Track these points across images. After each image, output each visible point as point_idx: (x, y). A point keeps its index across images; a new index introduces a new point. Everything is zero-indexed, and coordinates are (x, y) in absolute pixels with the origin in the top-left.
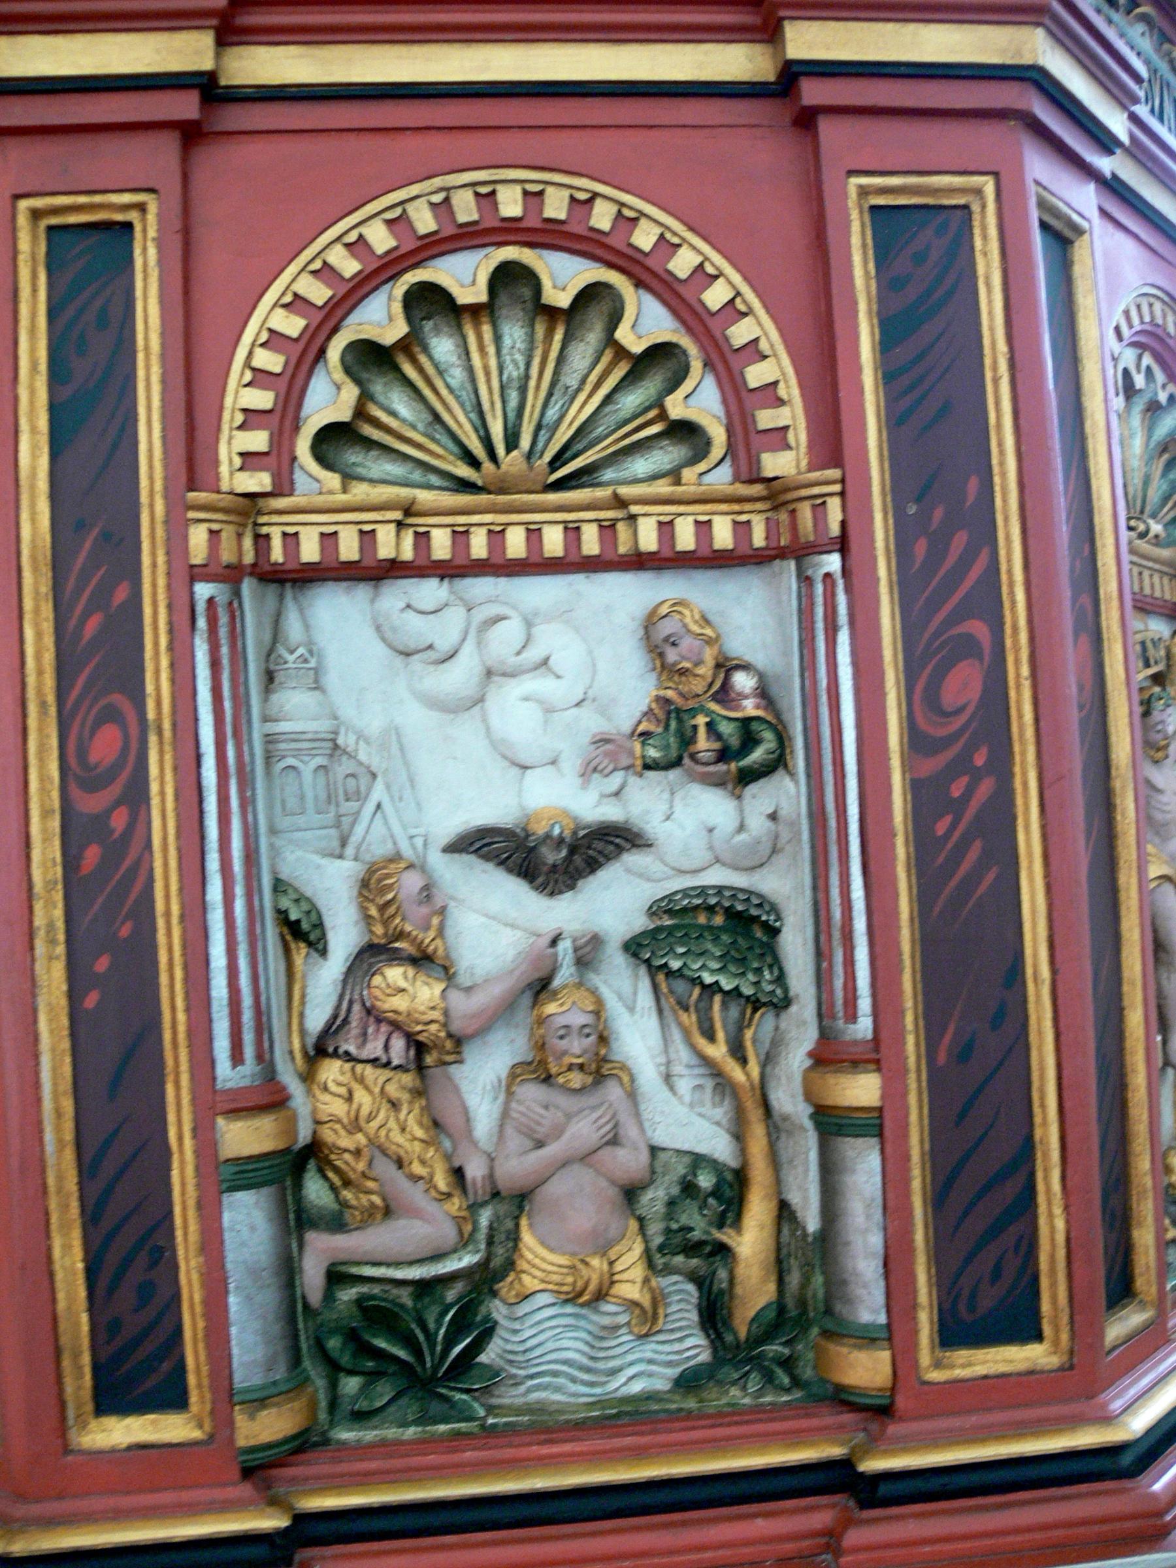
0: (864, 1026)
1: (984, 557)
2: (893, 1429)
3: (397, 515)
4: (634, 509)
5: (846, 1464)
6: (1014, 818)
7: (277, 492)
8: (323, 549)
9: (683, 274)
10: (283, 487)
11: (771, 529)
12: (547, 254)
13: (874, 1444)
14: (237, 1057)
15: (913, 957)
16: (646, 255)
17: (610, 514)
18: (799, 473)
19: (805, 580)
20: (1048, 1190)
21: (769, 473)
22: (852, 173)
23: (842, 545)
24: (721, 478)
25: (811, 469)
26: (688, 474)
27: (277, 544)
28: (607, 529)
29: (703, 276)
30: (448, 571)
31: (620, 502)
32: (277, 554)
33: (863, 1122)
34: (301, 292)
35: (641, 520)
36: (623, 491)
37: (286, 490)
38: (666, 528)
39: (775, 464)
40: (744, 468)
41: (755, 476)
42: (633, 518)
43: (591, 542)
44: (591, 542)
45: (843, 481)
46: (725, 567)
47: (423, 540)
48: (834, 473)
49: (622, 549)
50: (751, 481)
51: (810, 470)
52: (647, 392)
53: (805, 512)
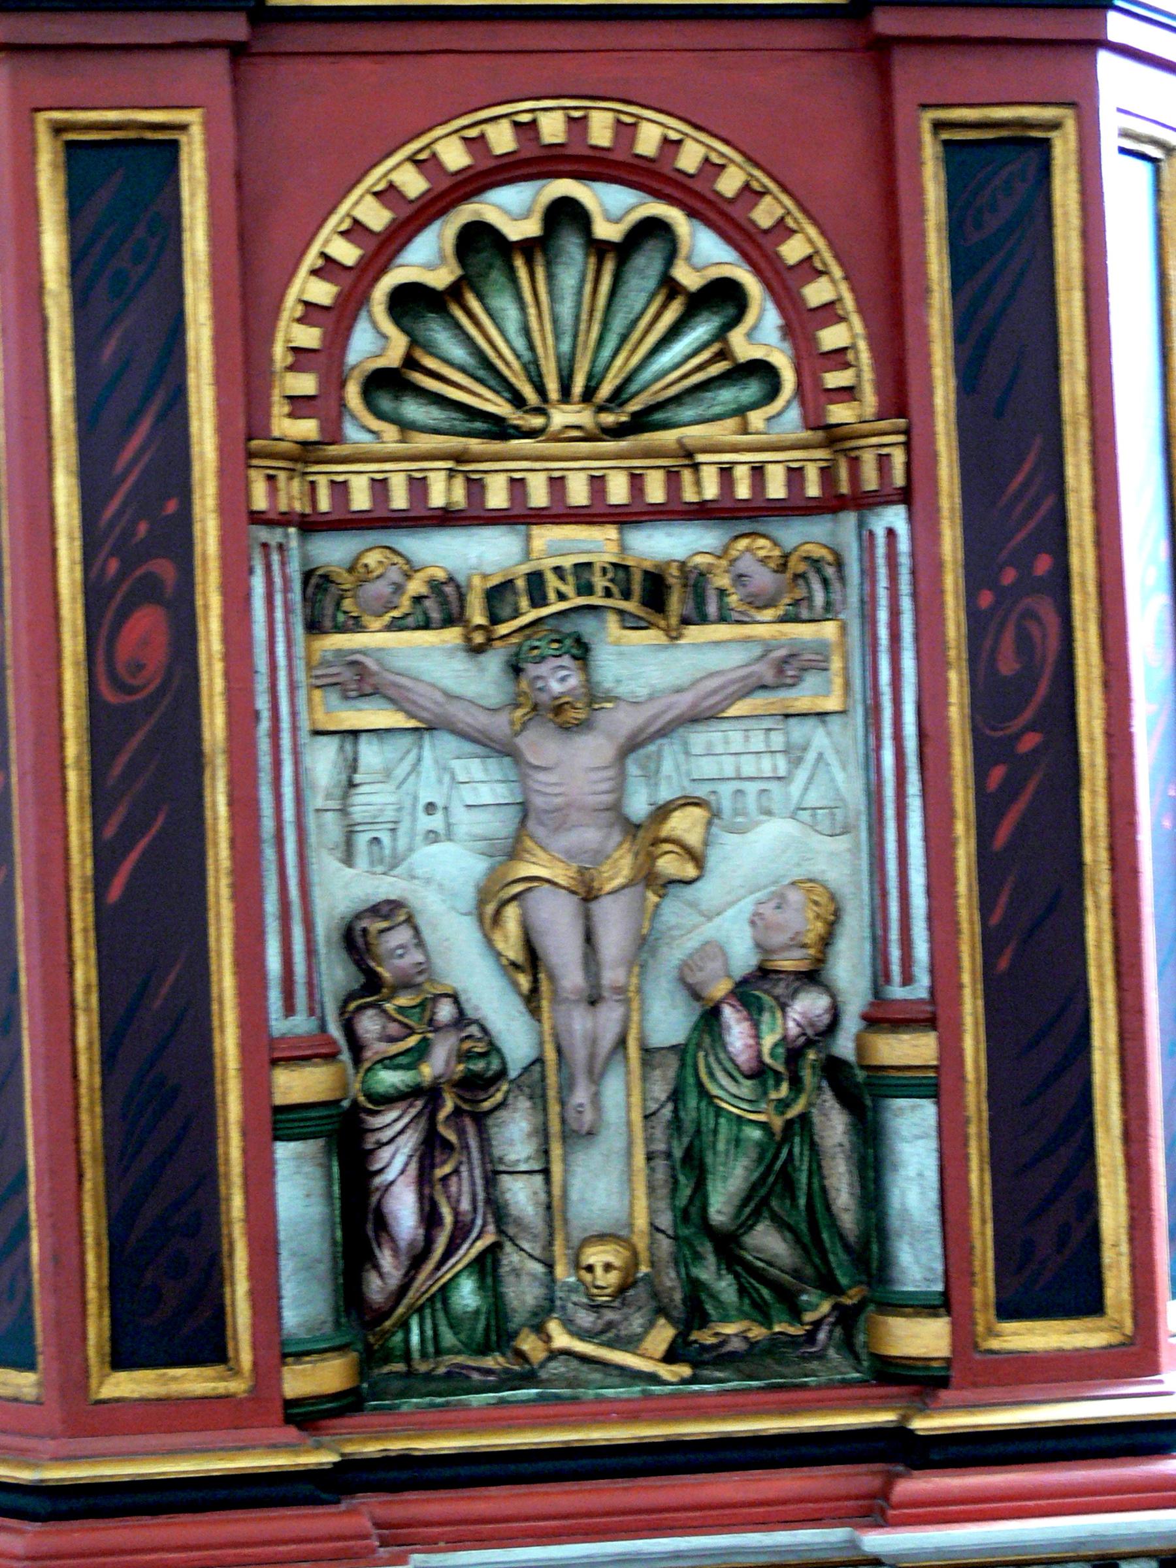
0: (921, 988)
1: (109, 832)
2: (944, 1395)
4: (701, 458)
6: (1068, 1426)
8: (512, 498)
9: (691, 170)
10: (333, 434)
11: (826, 475)
12: (599, 186)
14: (289, 1009)
15: (971, 922)
16: (691, 176)
20: (1087, 643)
21: (833, 420)
22: (925, 106)
23: (905, 496)
26: (756, 418)
28: (673, 477)
29: (712, 169)
33: (918, 1082)
35: (704, 468)
39: (840, 413)
40: (812, 418)
42: (696, 467)
43: (655, 492)
44: (655, 492)
45: (907, 432)
48: (901, 422)
51: (880, 418)
53: (869, 461)
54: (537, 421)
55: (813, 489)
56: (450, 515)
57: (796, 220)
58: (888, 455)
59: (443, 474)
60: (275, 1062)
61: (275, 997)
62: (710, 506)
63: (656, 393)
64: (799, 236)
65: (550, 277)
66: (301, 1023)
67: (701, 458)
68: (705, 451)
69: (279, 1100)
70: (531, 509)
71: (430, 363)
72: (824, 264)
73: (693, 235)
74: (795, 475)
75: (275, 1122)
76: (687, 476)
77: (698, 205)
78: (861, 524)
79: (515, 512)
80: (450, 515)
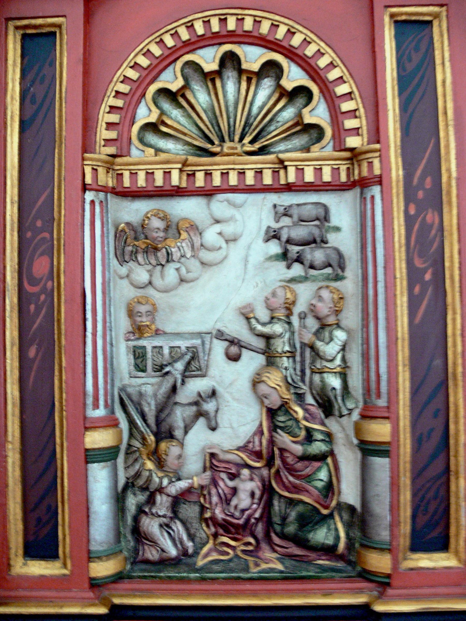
2: (390, 591)
3: (179, 166)
5: (366, 607)
7: (119, 154)
13: (381, 596)
17: (276, 166)
18: (363, 145)
19: (363, 199)
24: (329, 151)
25: (368, 144)
26: (315, 148)
27: (142, 176)
28: (275, 172)
30: (250, 190)
31: (281, 162)
32: (127, 182)
34: (138, 62)
36: (281, 156)
37: (125, 152)
38: (300, 171)
41: (343, 148)
42: (285, 168)
43: (268, 179)
46: (279, 192)
47: (167, 175)
48: (377, 146)
49: (283, 182)
50: (341, 150)
51: (368, 144)
52: (231, 79)
54: (218, 149)
55: (343, 178)
56: (180, 190)
57: (347, 78)
58: (372, 162)
59: (178, 170)
60: (87, 429)
61: (90, 401)
62: (291, 185)
63: (240, 126)
64: (347, 84)
65: (223, 87)
66: (101, 412)
67: (286, 163)
68: (287, 161)
69: (88, 446)
70: (215, 187)
71: (169, 122)
72: (337, 63)
73: (289, 67)
74: (336, 171)
75: (86, 455)
76: (282, 172)
77: (325, 90)
78: (362, 193)
79: (240, 187)
80: (180, 190)
